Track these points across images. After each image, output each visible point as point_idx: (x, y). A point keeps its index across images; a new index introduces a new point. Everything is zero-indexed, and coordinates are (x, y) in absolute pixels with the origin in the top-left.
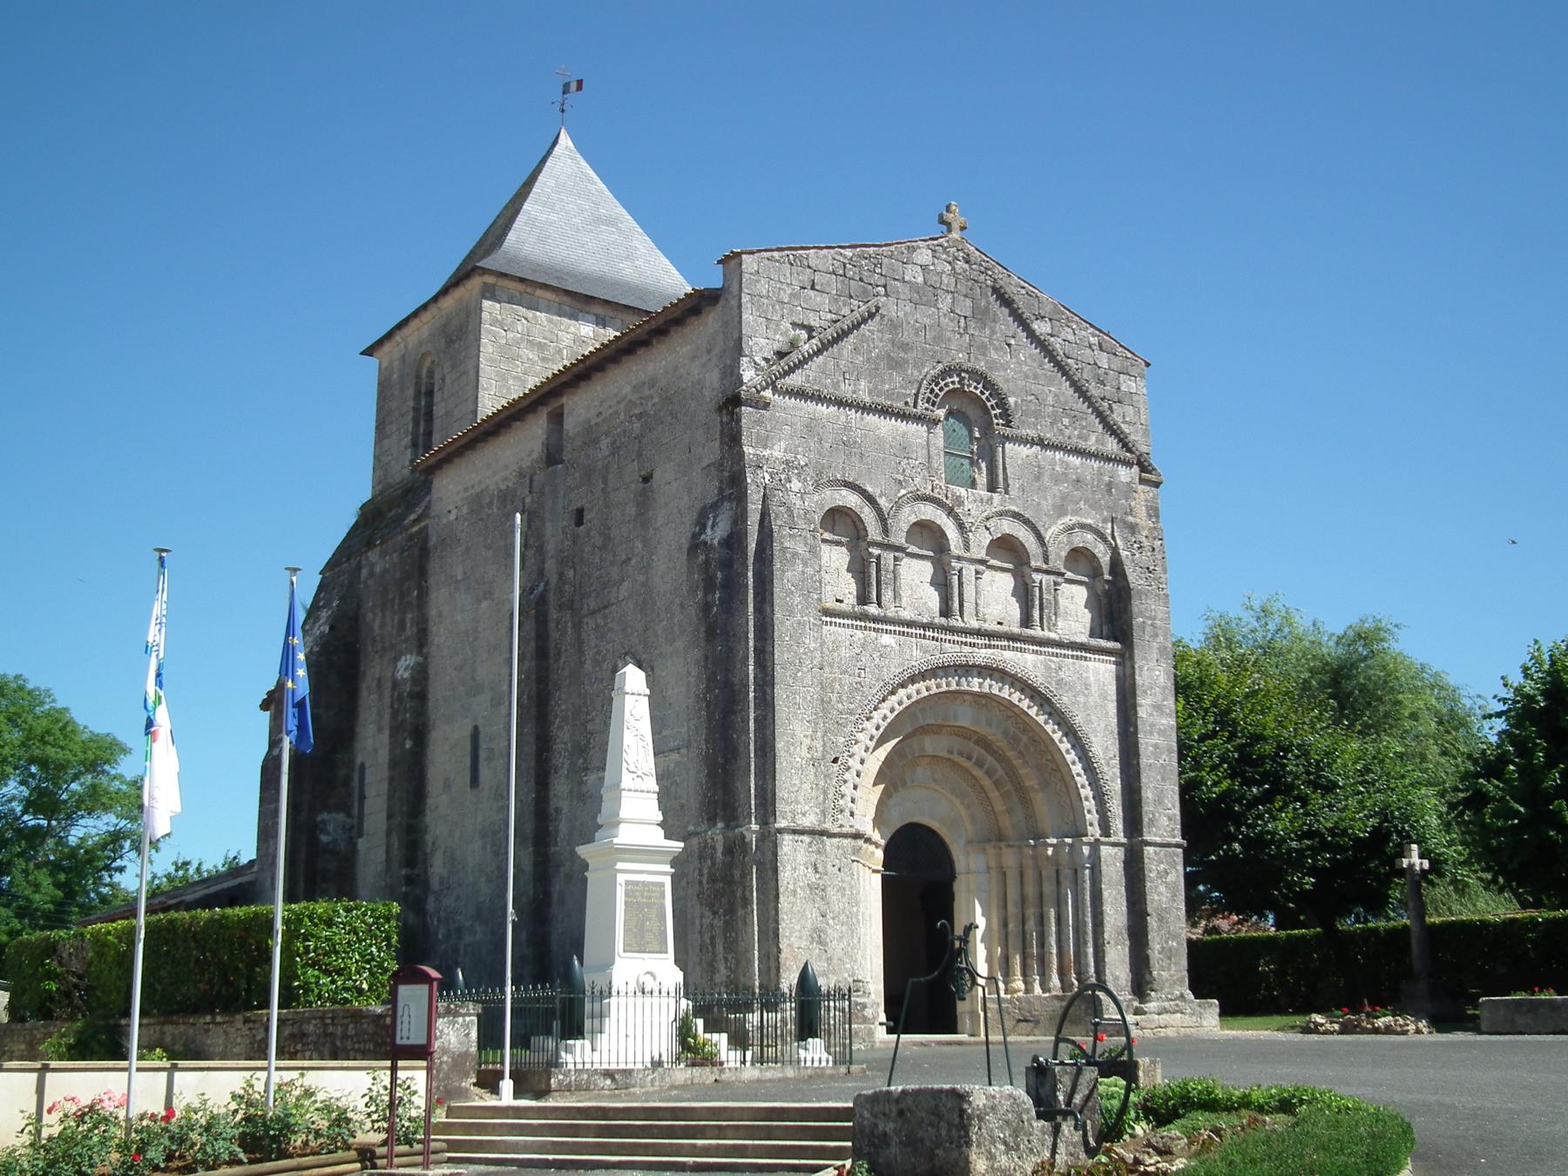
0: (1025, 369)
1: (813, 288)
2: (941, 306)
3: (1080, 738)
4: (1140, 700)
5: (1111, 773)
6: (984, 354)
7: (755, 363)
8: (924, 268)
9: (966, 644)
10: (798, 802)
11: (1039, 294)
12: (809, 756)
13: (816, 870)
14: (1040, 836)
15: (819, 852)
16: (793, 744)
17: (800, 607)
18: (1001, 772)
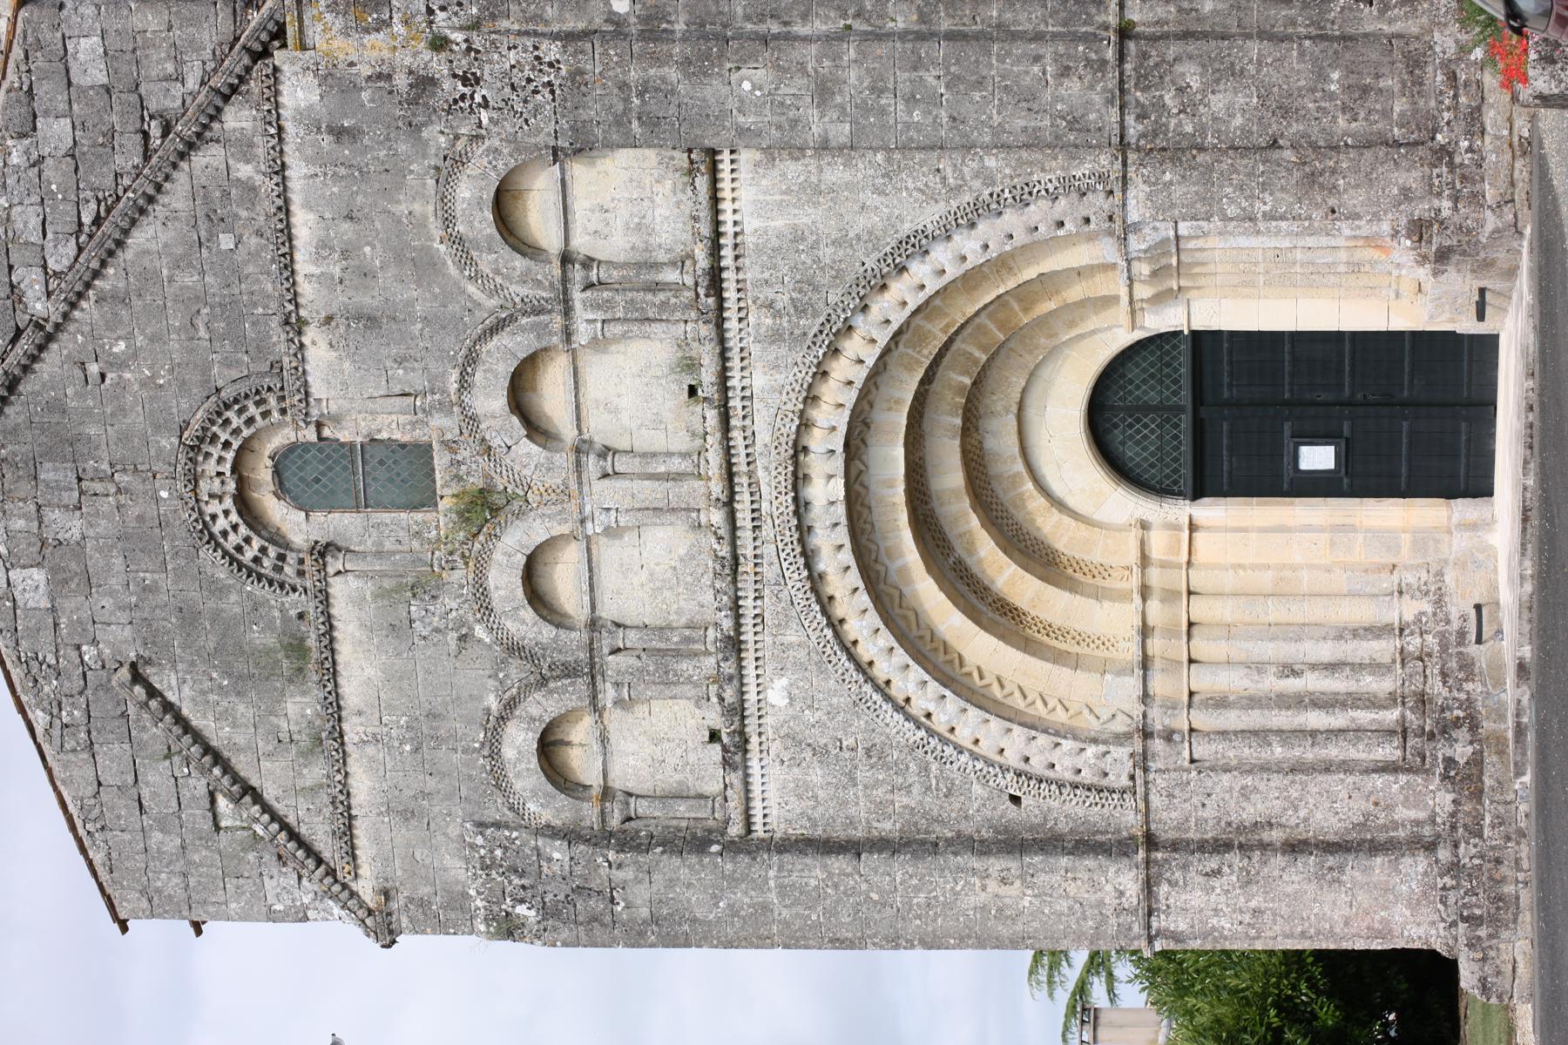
5: (977, 184)
10: (1101, 903)
12: (1018, 883)
16: (1000, 910)
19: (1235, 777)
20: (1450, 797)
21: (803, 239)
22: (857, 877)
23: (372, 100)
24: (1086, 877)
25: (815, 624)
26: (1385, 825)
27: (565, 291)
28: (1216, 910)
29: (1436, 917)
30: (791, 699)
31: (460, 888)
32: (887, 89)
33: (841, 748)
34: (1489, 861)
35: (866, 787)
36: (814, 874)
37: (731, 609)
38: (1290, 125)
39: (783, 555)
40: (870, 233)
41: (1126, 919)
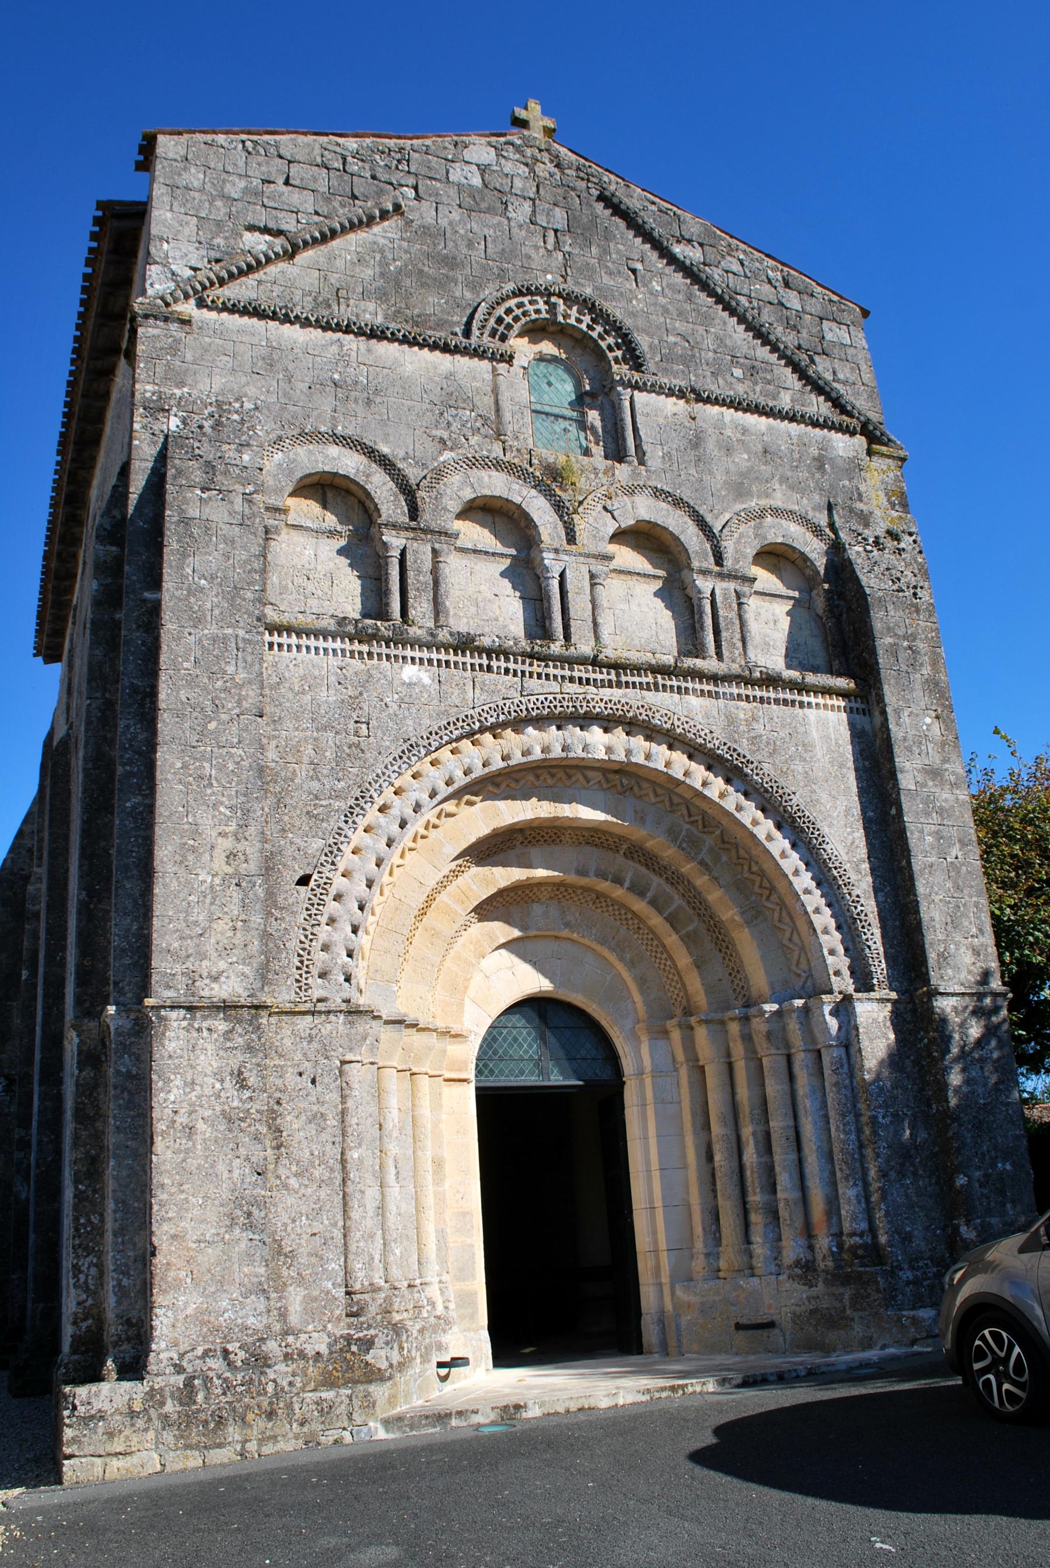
0: (662, 300)
1: (287, 183)
2: (512, 215)
3: (802, 830)
4: (901, 760)
6: (590, 278)
7: (173, 274)
8: (483, 169)
9: (572, 680)
11: (679, 212)
12: (230, 870)
13: (242, 1083)
14: (750, 1003)
15: (249, 1048)
16: (194, 850)
17: (216, 612)
18: (678, 901)
19: (336, 1107)
20: (323, 1349)
21: (806, 751)
22: (237, 711)
23: (844, 486)
24: (237, 942)
25: (485, 715)
26: (280, 1277)
27: (736, 577)
28: (193, 1083)
29: (183, 1348)
30: (410, 684)
31: (189, 381)
32: (943, 819)
33: (356, 722)
34: (271, 1403)
35: (316, 739)
36: (240, 670)
37: (500, 646)
38: (969, 1131)
39: (550, 697)
40: (817, 801)
41: (181, 982)
